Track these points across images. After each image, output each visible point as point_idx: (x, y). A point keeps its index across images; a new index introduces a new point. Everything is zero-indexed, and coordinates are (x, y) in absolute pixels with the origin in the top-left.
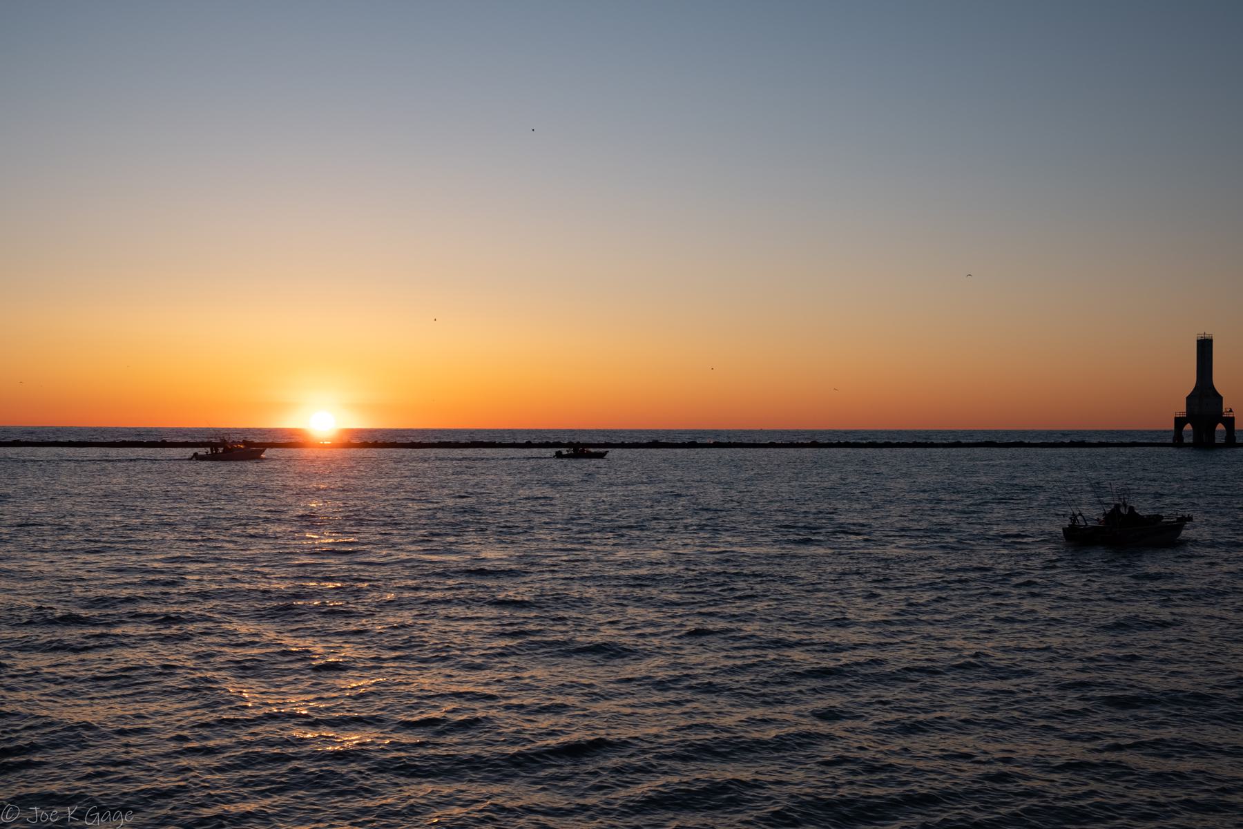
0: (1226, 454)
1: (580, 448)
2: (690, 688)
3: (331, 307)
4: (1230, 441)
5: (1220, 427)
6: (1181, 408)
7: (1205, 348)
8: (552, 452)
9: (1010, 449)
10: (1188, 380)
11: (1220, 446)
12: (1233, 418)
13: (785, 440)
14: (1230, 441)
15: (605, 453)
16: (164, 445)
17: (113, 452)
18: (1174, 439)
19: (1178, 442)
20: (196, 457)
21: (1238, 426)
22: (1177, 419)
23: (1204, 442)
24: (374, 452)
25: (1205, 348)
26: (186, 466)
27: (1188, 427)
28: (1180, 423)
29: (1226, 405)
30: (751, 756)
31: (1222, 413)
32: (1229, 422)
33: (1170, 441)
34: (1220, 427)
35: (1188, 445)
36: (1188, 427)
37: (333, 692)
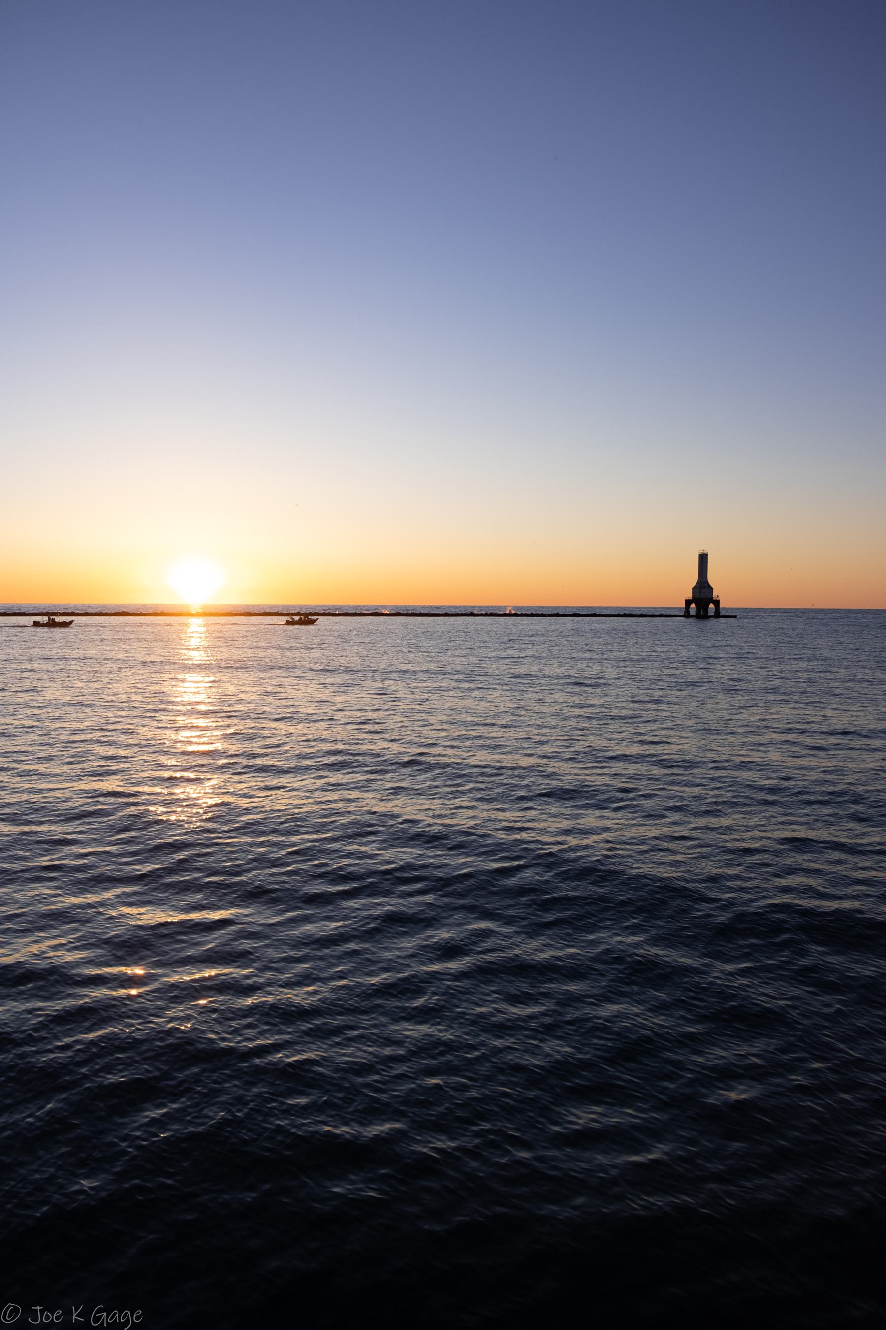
0: (713, 621)
5: (711, 606)
6: (689, 595)
7: (703, 559)
8: (283, 619)
10: (693, 579)
11: (693, 616)
13: (605, 612)
14: (717, 615)
15: (71, 622)
16: (162, 614)
19: (687, 615)
20: (36, 624)
21: (721, 606)
23: (703, 615)
24: (224, 619)
25: (703, 559)
26: (25, 634)
27: (693, 606)
29: (715, 593)
30: (117, 1043)
31: (712, 597)
32: (717, 603)
33: (682, 613)
34: (711, 606)
35: (693, 616)
36: (693, 606)
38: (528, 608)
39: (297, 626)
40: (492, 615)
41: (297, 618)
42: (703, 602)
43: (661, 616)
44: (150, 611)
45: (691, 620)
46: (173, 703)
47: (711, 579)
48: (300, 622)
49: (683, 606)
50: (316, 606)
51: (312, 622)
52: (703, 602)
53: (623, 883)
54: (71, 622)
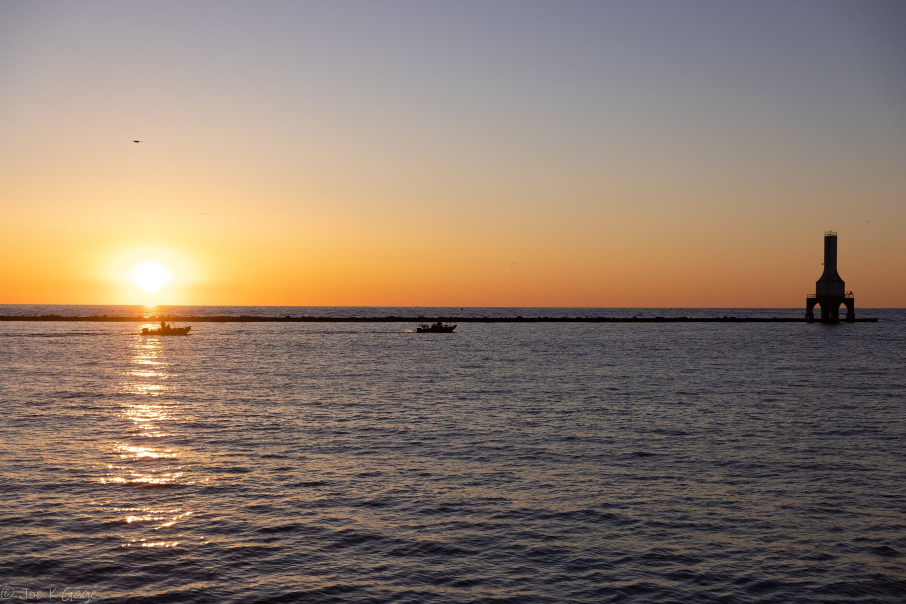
1: (438, 323)
2: (830, 492)
3: (163, 226)
4: (851, 318)
5: (843, 306)
6: (812, 291)
7: (831, 242)
9: (322, 323)
10: (818, 270)
11: (817, 320)
12: (853, 299)
14: (851, 318)
16: (105, 319)
17: (328, 326)
18: (806, 315)
19: (809, 318)
21: (856, 306)
22: (808, 300)
23: (830, 319)
25: (831, 242)
27: (817, 306)
28: (811, 302)
29: (847, 289)
32: (850, 302)
34: (843, 306)
35: (817, 320)
36: (817, 306)
37: (144, 446)
38: (542, 310)
39: (430, 334)
40: (733, 320)
41: (430, 325)
42: (830, 300)
43: (635, 318)
44: (101, 315)
45: (813, 328)
46: (101, 396)
47: (842, 270)
48: (434, 330)
49: (804, 306)
50: (590, 309)
51: (450, 330)
52: (830, 300)
53: (63, 573)
54: (189, 329)
